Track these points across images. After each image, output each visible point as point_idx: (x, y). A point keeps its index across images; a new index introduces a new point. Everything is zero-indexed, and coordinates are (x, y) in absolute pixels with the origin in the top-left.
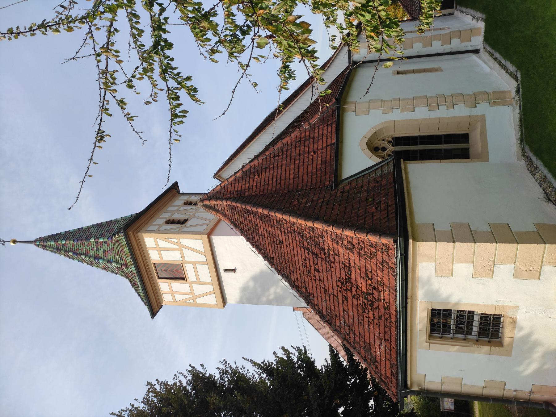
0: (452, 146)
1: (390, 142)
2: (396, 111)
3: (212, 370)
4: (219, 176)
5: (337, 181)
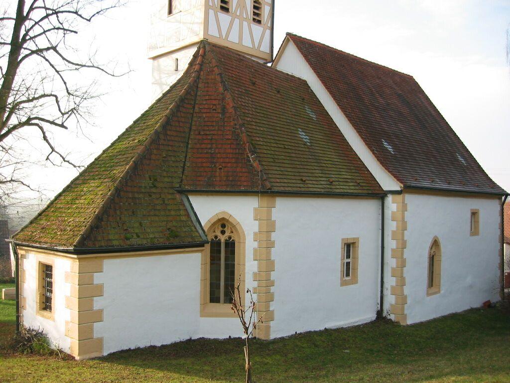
0: (222, 286)
1: (230, 238)
2: (256, 245)
3: (327, 328)
4: (288, 39)
5: (185, 193)
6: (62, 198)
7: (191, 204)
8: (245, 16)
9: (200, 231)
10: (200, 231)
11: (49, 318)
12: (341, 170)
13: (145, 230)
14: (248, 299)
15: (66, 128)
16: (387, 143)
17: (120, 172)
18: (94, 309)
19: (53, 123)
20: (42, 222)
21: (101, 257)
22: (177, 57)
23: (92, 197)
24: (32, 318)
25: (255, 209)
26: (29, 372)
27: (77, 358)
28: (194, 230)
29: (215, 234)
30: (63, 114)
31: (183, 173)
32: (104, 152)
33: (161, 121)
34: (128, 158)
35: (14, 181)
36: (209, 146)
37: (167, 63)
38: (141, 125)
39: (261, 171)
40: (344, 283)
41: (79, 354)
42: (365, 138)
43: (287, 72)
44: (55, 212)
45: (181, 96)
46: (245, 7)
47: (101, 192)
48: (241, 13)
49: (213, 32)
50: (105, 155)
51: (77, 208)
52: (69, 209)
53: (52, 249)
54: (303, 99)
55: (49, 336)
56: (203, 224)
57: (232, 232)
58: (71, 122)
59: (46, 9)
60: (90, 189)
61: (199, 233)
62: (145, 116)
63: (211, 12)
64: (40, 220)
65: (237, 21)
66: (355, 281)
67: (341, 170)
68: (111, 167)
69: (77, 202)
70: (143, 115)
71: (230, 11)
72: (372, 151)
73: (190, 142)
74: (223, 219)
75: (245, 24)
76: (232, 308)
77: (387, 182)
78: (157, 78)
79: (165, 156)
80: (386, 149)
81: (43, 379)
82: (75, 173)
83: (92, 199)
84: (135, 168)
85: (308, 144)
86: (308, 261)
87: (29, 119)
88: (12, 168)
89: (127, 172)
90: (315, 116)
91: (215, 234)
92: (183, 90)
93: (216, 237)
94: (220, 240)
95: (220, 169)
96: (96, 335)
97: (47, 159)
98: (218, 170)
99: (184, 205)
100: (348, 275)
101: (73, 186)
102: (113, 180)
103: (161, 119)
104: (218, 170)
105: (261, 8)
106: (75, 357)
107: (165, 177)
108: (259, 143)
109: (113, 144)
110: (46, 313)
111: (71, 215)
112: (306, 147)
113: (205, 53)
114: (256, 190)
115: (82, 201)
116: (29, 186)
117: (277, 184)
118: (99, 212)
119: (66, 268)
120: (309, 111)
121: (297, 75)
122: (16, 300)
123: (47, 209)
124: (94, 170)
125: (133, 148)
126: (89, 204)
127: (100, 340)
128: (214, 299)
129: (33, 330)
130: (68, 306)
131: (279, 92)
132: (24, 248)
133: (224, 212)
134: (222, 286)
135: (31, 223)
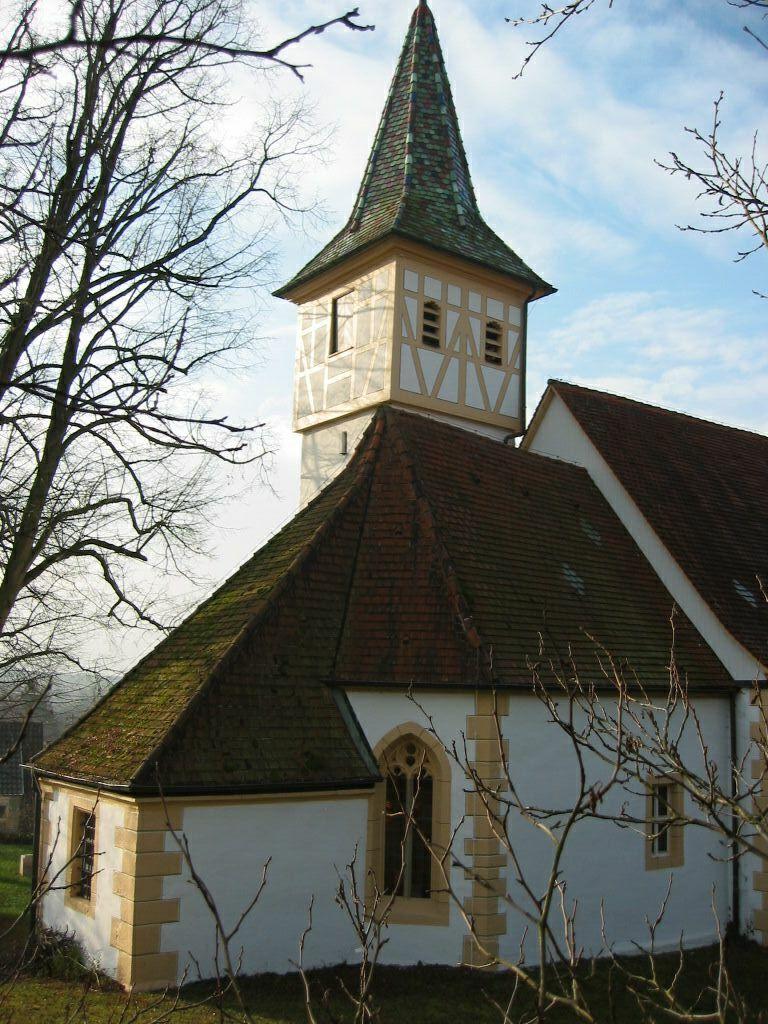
0: (406, 866)
5: (341, 686)
6: (122, 691)
7: (350, 708)
8: (469, 353)
9: (367, 758)
10: (367, 758)
11: (87, 912)
12: (646, 642)
13: (262, 754)
14: (461, 885)
15: (144, 559)
16: (745, 586)
17: (221, 647)
18: (164, 898)
19: (120, 550)
20: (83, 735)
21: (178, 802)
22: (346, 430)
23: (171, 692)
24: (59, 913)
25: (469, 719)
26: (35, 1006)
27: (128, 988)
28: (355, 755)
29: (395, 764)
30: (141, 533)
31: (337, 649)
32: (201, 608)
33: (298, 555)
34: (238, 621)
35: (51, 652)
36: (387, 600)
37: (329, 440)
38: (266, 561)
39: (480, 647)
40: (652, 865)
41: (134, 981)
42: (696, 579)
43: (546, 455)
44: (108, 717)
45: (338, 508)
46: (469, 335)
47: (187, 684)
48: (463, 346)
49: (410, 384)
50: (200, 615)
51: (145, 711)
52: (132, 712)
53: (95, 786)
54: (577, 506)
55: (86, 945)
56: (373, 745)
57: (428, 761)
58: (155, 548)
59: (117, 348)
60: (170, 678)
61: (364, 762)
62: (275, 543)
63: (406, 349)
64: (82, 730)
65: (454, 363)
66: (677, 861)
67: (646, 642)
68: (209, 638)
69: (146, 700)
70: (271, 542)
71: (441, 344)
72: (710, 603)
73: (353, 592)
74: (410, 736)
75: (471, 367)
76: (337, 900)
77: (739, 664)
78: (312, 468)
79: (304, 618)
80: (741, 599)
81: (59, 1019)
82: (158, 637)
83: (170, 696)
84: (246, 644)
85: (581, 592)
86: (556, 812)
87: (79, 544)
88: (47, 629)
89: (234, 649)
90: (599, 538)
91: (395, 764)
92: (343, 498)
93: (398, 769)
94: (404, 775)
95: (406, 643)
96: (165, 947)
97: (111, 614)
98: (402, 645)
99: (339, 711)
100: (663, 848)
101: (142, 670)
102: (209, 661)
103: (300, 551)
104: (402, 645)
105: (500, 336)
106: (124, 987)
107: (302, 657)
108: (480, 593)
109: (216, 595)
110: (81, 902)
111: (132, 724)
112: (576, 598)
113: (385, 428)
114: (469, 682)
115: (153, 699)
116: (77, 663)
117: (512, 672)
118: (179, 722)
119: (116, 818)
120: (587, 529)
121: (567, 458)
122: (36, 879)
123: (94, 710)
124: (181, 642)
125: (248, 604)
126: (164, 704)
127: (173, 957)
128: (391, 884)
129: (57, 933)
130: (118, 892)
131: (527, 494)
132: (50, 781)
133: (411, 724)
134: (406, 866)
135: (67, 735)
